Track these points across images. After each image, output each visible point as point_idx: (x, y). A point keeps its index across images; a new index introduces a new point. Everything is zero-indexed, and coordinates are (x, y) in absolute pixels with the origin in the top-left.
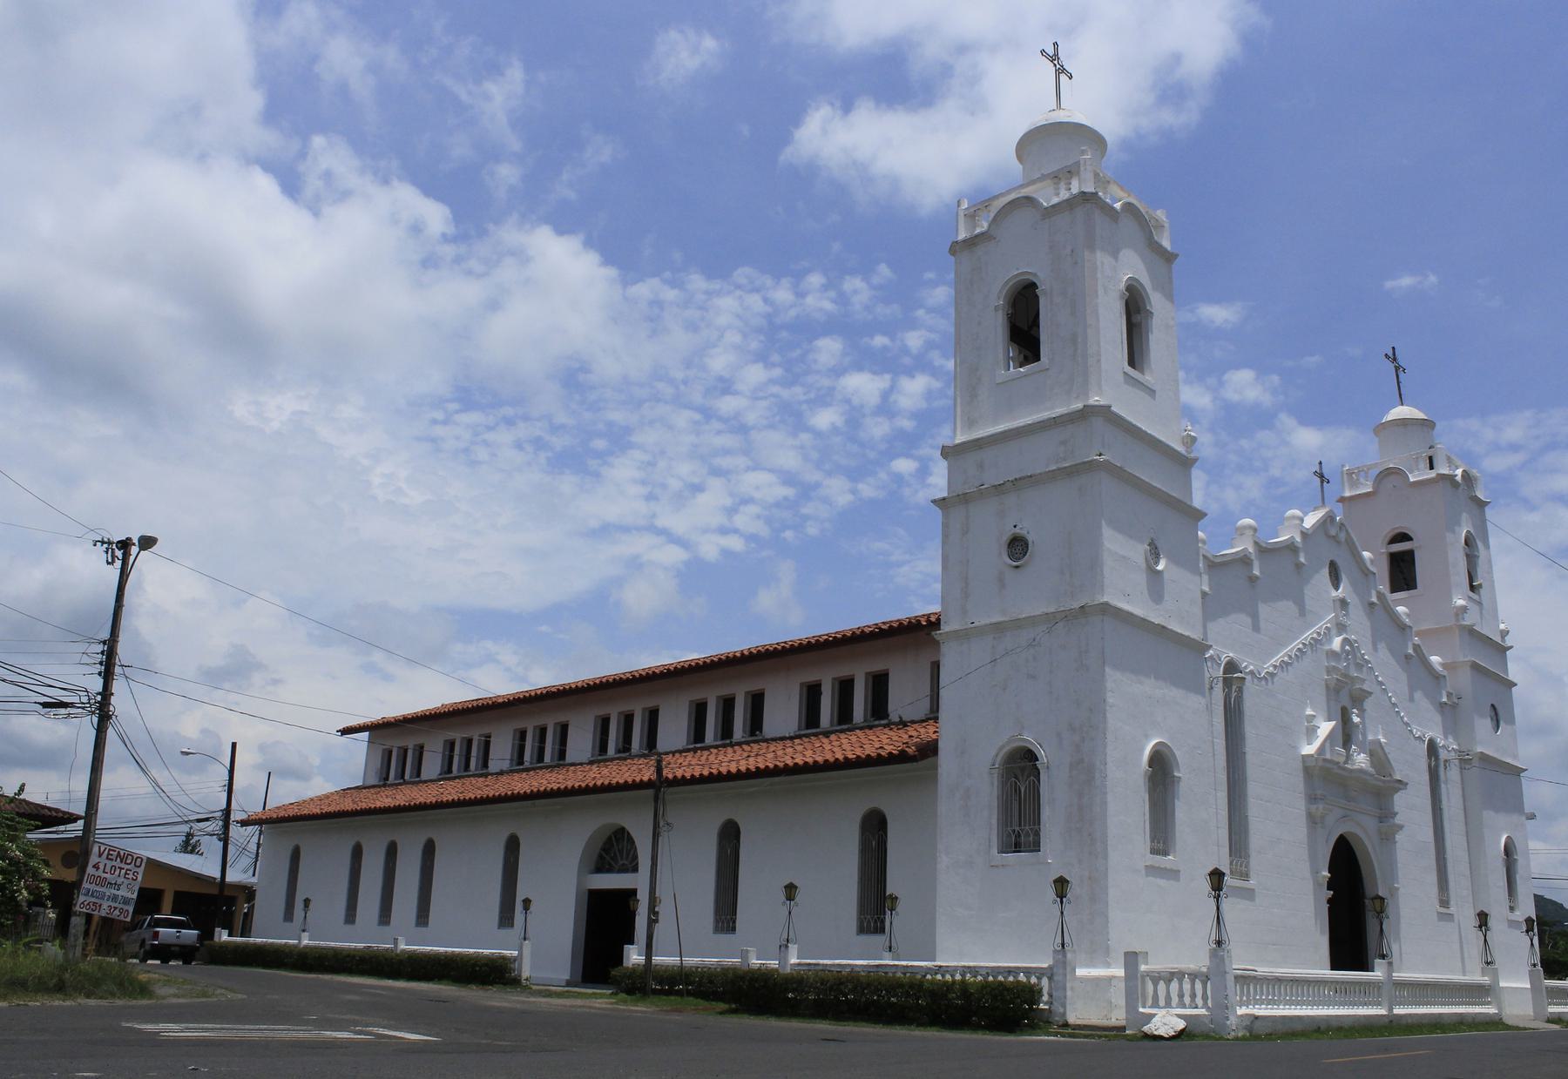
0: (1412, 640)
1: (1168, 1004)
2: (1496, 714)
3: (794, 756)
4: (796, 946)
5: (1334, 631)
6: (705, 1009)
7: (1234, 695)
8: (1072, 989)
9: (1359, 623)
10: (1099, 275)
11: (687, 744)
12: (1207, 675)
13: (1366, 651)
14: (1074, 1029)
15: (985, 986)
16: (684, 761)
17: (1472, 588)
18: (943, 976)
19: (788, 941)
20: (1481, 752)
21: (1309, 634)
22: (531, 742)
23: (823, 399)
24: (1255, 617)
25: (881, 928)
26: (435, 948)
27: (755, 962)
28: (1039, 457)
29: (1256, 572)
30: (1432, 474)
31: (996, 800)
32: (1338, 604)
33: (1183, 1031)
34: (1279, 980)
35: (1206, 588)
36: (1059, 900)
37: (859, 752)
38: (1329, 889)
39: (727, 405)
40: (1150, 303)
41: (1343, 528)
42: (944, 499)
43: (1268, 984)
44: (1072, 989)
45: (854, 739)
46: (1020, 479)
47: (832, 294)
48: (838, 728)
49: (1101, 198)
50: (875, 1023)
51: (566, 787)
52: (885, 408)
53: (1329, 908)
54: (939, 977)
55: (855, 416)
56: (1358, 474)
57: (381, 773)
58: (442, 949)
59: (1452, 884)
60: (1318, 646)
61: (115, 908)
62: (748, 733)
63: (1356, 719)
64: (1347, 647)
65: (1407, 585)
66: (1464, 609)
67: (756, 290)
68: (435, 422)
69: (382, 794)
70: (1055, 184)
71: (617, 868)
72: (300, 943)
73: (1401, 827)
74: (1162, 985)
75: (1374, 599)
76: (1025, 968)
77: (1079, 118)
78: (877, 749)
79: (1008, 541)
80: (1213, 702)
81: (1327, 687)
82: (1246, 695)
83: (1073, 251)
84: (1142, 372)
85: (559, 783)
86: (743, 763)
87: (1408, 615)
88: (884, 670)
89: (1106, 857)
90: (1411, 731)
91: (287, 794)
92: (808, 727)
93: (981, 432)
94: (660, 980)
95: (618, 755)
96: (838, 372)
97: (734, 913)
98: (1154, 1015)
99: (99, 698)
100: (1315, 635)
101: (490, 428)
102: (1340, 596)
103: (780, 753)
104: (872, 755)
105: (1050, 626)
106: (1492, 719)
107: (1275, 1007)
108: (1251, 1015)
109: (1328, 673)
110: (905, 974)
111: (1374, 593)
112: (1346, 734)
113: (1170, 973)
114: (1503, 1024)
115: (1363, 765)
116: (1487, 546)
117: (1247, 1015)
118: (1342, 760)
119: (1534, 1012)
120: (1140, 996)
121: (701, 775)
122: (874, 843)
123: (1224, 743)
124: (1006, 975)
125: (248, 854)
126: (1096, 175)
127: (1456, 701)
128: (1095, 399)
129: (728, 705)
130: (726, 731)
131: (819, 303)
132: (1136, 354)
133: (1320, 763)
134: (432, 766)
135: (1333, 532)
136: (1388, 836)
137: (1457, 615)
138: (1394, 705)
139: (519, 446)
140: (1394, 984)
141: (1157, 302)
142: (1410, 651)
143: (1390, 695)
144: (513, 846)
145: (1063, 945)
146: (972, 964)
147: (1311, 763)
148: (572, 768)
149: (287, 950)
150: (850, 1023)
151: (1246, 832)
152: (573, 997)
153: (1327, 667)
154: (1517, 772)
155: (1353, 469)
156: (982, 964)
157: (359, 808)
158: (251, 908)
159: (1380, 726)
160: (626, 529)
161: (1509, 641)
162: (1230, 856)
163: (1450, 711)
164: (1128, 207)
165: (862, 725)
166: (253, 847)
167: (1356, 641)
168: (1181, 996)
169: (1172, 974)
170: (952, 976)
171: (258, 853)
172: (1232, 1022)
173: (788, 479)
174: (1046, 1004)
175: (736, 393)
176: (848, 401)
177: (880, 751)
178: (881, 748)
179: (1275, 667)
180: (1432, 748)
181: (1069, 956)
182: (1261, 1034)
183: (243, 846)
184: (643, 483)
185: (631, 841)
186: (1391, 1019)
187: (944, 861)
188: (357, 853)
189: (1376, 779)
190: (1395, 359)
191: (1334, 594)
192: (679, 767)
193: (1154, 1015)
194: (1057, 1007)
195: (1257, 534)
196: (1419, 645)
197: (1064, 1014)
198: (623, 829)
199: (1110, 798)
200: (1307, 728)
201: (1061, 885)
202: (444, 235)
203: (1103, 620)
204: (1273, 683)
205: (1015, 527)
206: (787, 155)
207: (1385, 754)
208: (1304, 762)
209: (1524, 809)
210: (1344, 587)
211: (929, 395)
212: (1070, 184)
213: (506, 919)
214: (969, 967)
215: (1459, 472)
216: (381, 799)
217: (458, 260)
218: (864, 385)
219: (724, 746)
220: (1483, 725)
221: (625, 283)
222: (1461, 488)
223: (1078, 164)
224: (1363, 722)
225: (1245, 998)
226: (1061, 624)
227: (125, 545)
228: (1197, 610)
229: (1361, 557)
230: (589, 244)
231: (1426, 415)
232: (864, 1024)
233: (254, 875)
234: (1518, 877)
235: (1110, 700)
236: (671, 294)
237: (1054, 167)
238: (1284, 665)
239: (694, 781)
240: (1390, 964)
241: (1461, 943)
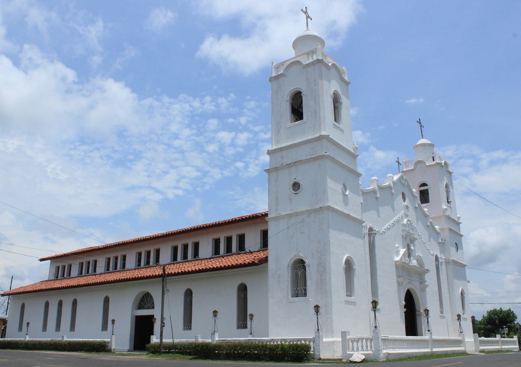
0: (429, 220)
1: (358, 350)
2: (457, 246)
3: (212, 265)
4: (218, 333)
5: (404, 217)
6: (184, 358)
7: (372, 239)
8: (322, 346)
9: (412, 212)
10: (324, 89)
11: (171, 262)
12: (363, 232)
13: (415, 224)
14: (323, 361)
15: (290, 346)
16: (171, 268)
17: (448, 202)
18: (274, 343)
19: (215, 332)
20: (453, 259)
21: (396, 218)
22: (120, 261)
23: (210, 141)
24: (378, 211)
25: (245, 327)
26: (78, 339)
27: (200, 340)
28: (303, 154)
29: (378, 196)
30: (434, 163)
31: (290, 278)
32: (405, 207)
33: (364, 359)
34: (396, 340)
35: (362, 201)
36: (316, 313)
37: (237, 262)
38: (404, 308)
39: (177, 143)
40: (341, 100)
41: (406, 181)
42: (269, 169)
43: (392, 342)
44: (322, 346)
45: (233, 258)
46: (297, 162)
47: (214, 104)
48: (227, 254)
49: (324, 62)
50: (249, 361)
51: (127, 278)
52: (233, 144)
53: (405, 315)
54: (272, 343)
55: (222, 148)
56: (408, 163)
57: (55, 276)
58: (81, 340)
59: (444, 306)
60: (399, 222)
62: (193, 257)
63: (412, 248)
64: (409, 223)
65: (426, 201)
66: (446, 209)
67: (188, 102)
68: (71, 149)
69: (56, 283)
70: (307, 56)
71: (146, 307)
72: (25, 339)
73: (428, 286)
74: (355, 343)
75: (417, 206)
76: (304, 339)
77: (315, 33)
78: (243, 261)
79: (293, 184)
80: (365, 242)
81: (403, 237)
82: (376, 239)
83: (314, 80)
84: (339, 123)
85: (124, 277)
86: (199, 266)
87: (428, 212)
88: (244, 233)
89: (331, 298)
90: (430, 252)
92: (215, 255)
93: (282, 145)
94: (165, 348)
95: (144, 267)
96: (216, 131)
97: (191, 323)
98: (353, 354)
100: (398, 218)
101: (91, 151)
102: (406, 204)
103: (207, 264)
104: (242, 263)
105: (309, 214)
106: (456, 248)
107: (395, 350)
108: (387, 353)
109: (403, 232)
110: (259, 342)
111: (417, 204)
112: (409, 253)
113: (358, 338)
114: (467, 353)
115: (415, 264)
116: (453, 188)
117: (386, 353)
118: (408, 262)
120: (347, 347)
121: (178, 272)
122: (242, 296)
123: (369, 256)
124: (297, 341)
125: (4, 307)
126: (323, 53)
127: (444, 241)
128: (323, 133)
129: (186, 247)
130: (185, 257)
131: (209, 107)
132: (337, 117)
133: (401, 263)
134: (75, 271)
135: (403, 182)
136: (423, 290)
137: (444, 212)
138: (424, 243)
139: (102, 158)
140: (433, 340)
141: (344, 99)
142: (429, 224)
143: (423, 239)
144: (107, 301)
145: (318, 330)
146: (284, 338)
147: (398, 263)
148: (128, 271)
149: (20, 342)
150: (240, 361)
151: (377, 288)
152: (132, 355)
153: (402, 230)
154: (464, 266)
155: (406, 161)
156: (288, 338)
157: (48, 288)
158: (5, 328)
159: (420, 251)
160: (140, 188)
161: (460, 221)
162: (372, 296)
163: (442, 245)
164: (334, 65)
165: (235, 253)
166: (6, 304)
167: (411, 221)
168: (362, 347)
169: (359, 339)
170: (277, 342)
171: (8, 306)
172: (382, 355)
173: (199, 169)
174: (312, 351)
175: (179, 139)
176: (220, 142)
177: (245, 262)
178: (245, 261)
179: (385, 229)
180: (437, 258)
181: (321, 334)
182: (392, 360)
183: (2, 304)
184: (146, 171)
185: (151, 297)
186: (432, 353)
187: (271, 301)
188: (47, 305)
189: (420, 269)
190: (420, 123)
191: (404, 204)
192: (173, 269)
193: (353, 354)
194: (317, 353)
195: (378, 182)
196: (431, 222)
197: (319, 355)
198: (148, 293)
199: (332, 276)
200: (396, 251)
201: (317, 308)
202: (74, 81)
203: (328, 212)
204: (385, 235)
205: (295, 179)
206: (198, 54)
207: (422, 260)
208: (395, 263)
209: (466, 279)
210: (407, 201)
211: (248, 140)
212: (313, 56)
213: (105, 327)
214: (283, 339)
215: (443, 162)
216: (56, 285)
217: (79, 90)
218: (225, 136)
219: (185, 262)
220: (453, 249)
221: (140, 99)
222: (444, 168)
223: (316, 49)
224: (414, 249)
225: (385, 347)
226: (313, 214)
228: (359, 208)
229: (412, 191)
230: (127, 85)
231: (431, 141)
232: (245, 361)
233: (6, 315)
234: (465, 303)
235: (331, 241)
236: (156, 104)
237: (307, 50)
238: (388, 229)
239: (176, 274)
240: (431, 333)
241: (448, 326)
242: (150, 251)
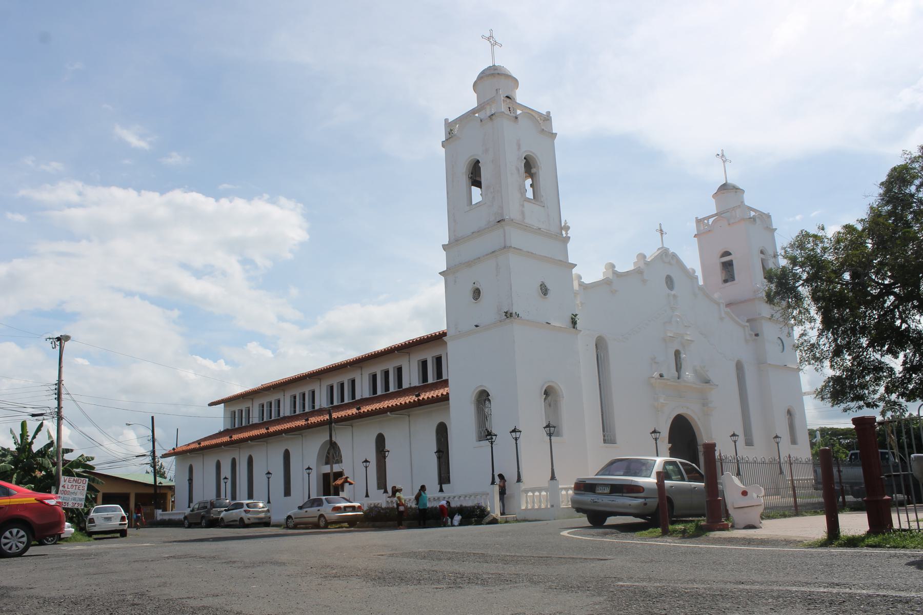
38: (669, 443)
53: (670, 453)
61: (75, 503)
91: (188, 438)
99: (56, 410)
119: (382, 489)
227: (59, 339)
242: (427, 360)
